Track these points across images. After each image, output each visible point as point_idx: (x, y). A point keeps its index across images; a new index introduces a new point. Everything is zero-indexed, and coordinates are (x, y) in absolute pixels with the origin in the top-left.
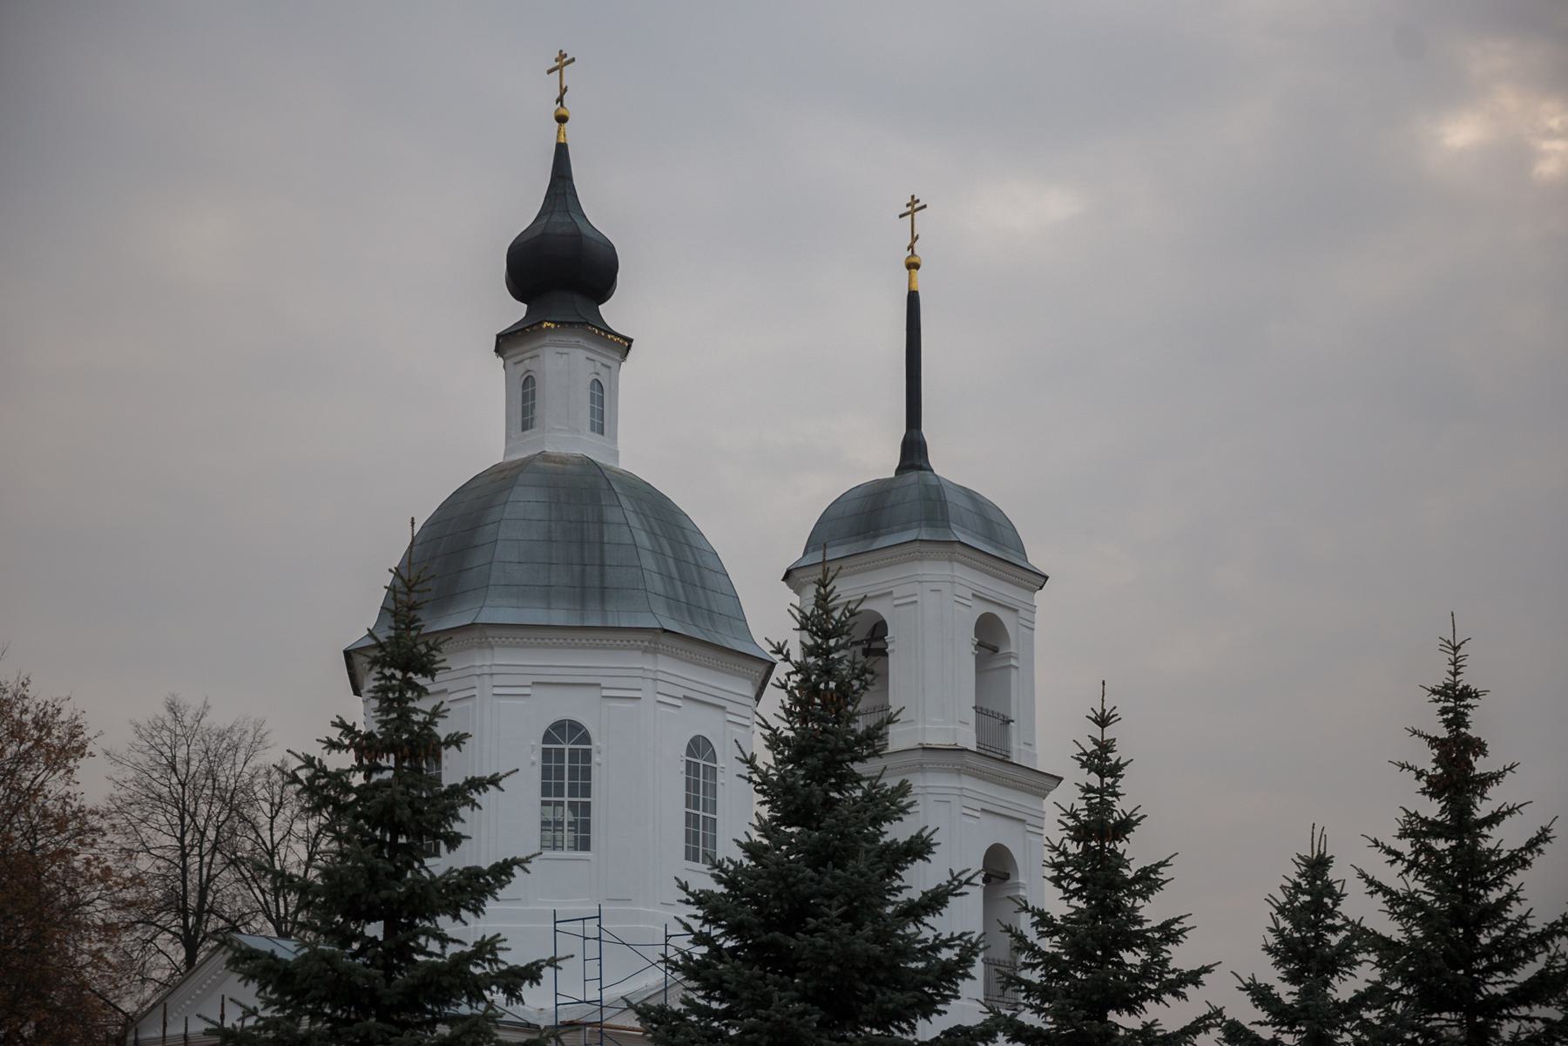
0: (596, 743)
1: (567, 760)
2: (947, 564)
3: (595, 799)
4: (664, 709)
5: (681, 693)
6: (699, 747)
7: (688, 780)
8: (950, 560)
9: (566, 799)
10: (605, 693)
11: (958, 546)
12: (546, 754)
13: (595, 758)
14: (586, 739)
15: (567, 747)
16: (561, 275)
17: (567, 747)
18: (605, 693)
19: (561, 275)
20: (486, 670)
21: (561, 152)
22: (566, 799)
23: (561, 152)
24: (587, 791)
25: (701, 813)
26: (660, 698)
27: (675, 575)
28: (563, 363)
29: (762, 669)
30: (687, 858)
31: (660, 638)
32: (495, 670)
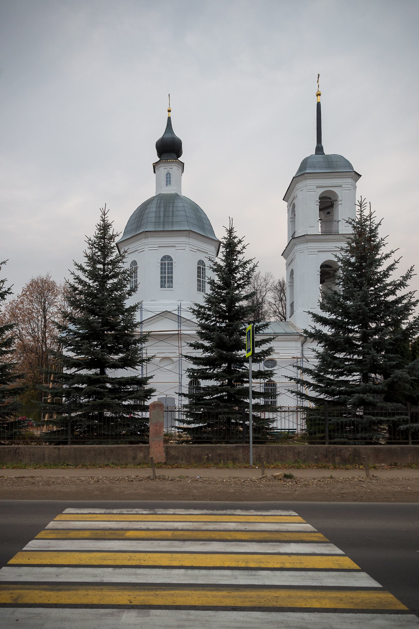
0: (174, 261)
1: (167, 265)
2: (305, 181)
3: (174, 275)
4: (192, 252)
5: (196, 248)
6: (201, 262)
7: (198, 271)
8: (306, 179)
9: (167, 275)
10: (177, 248)
11: (305, 174)
12: (162, 264)
13: (174, 265)
14: (172, 260)
15: (167, 262)
16: (169, 149)
17: (167, 262)
18: (177, 248)
19: (169, 149)
20: (146, 244)
21: (169, 119)
22: (167, 275)
23: (169, 119)
24: (161, 277)
25: (201, 279)
26: (149, 249)
27: (341, 378)
28: (174, 169)
29: (217, 244)
30: (198, 290)
31: (189, 233)
32: (149, 243)
